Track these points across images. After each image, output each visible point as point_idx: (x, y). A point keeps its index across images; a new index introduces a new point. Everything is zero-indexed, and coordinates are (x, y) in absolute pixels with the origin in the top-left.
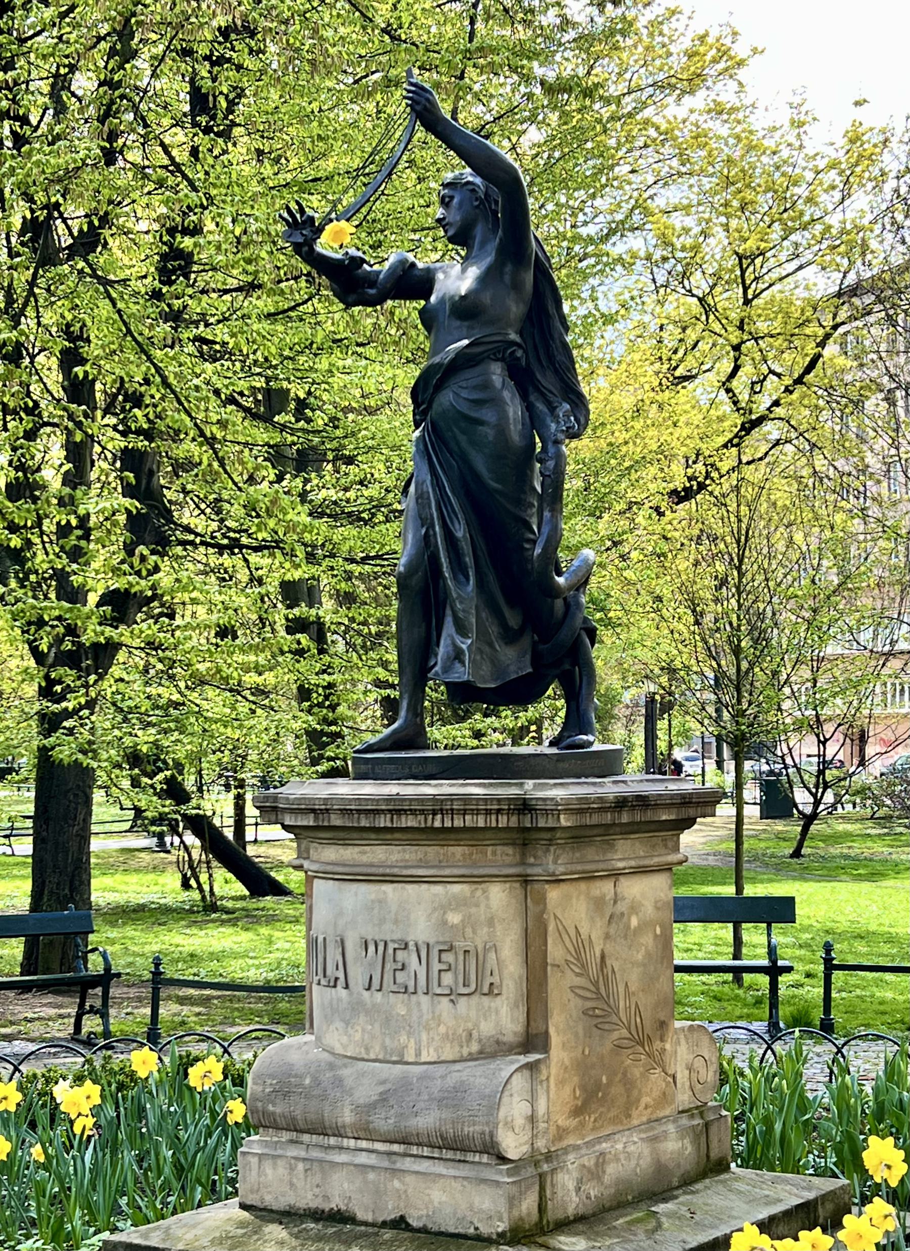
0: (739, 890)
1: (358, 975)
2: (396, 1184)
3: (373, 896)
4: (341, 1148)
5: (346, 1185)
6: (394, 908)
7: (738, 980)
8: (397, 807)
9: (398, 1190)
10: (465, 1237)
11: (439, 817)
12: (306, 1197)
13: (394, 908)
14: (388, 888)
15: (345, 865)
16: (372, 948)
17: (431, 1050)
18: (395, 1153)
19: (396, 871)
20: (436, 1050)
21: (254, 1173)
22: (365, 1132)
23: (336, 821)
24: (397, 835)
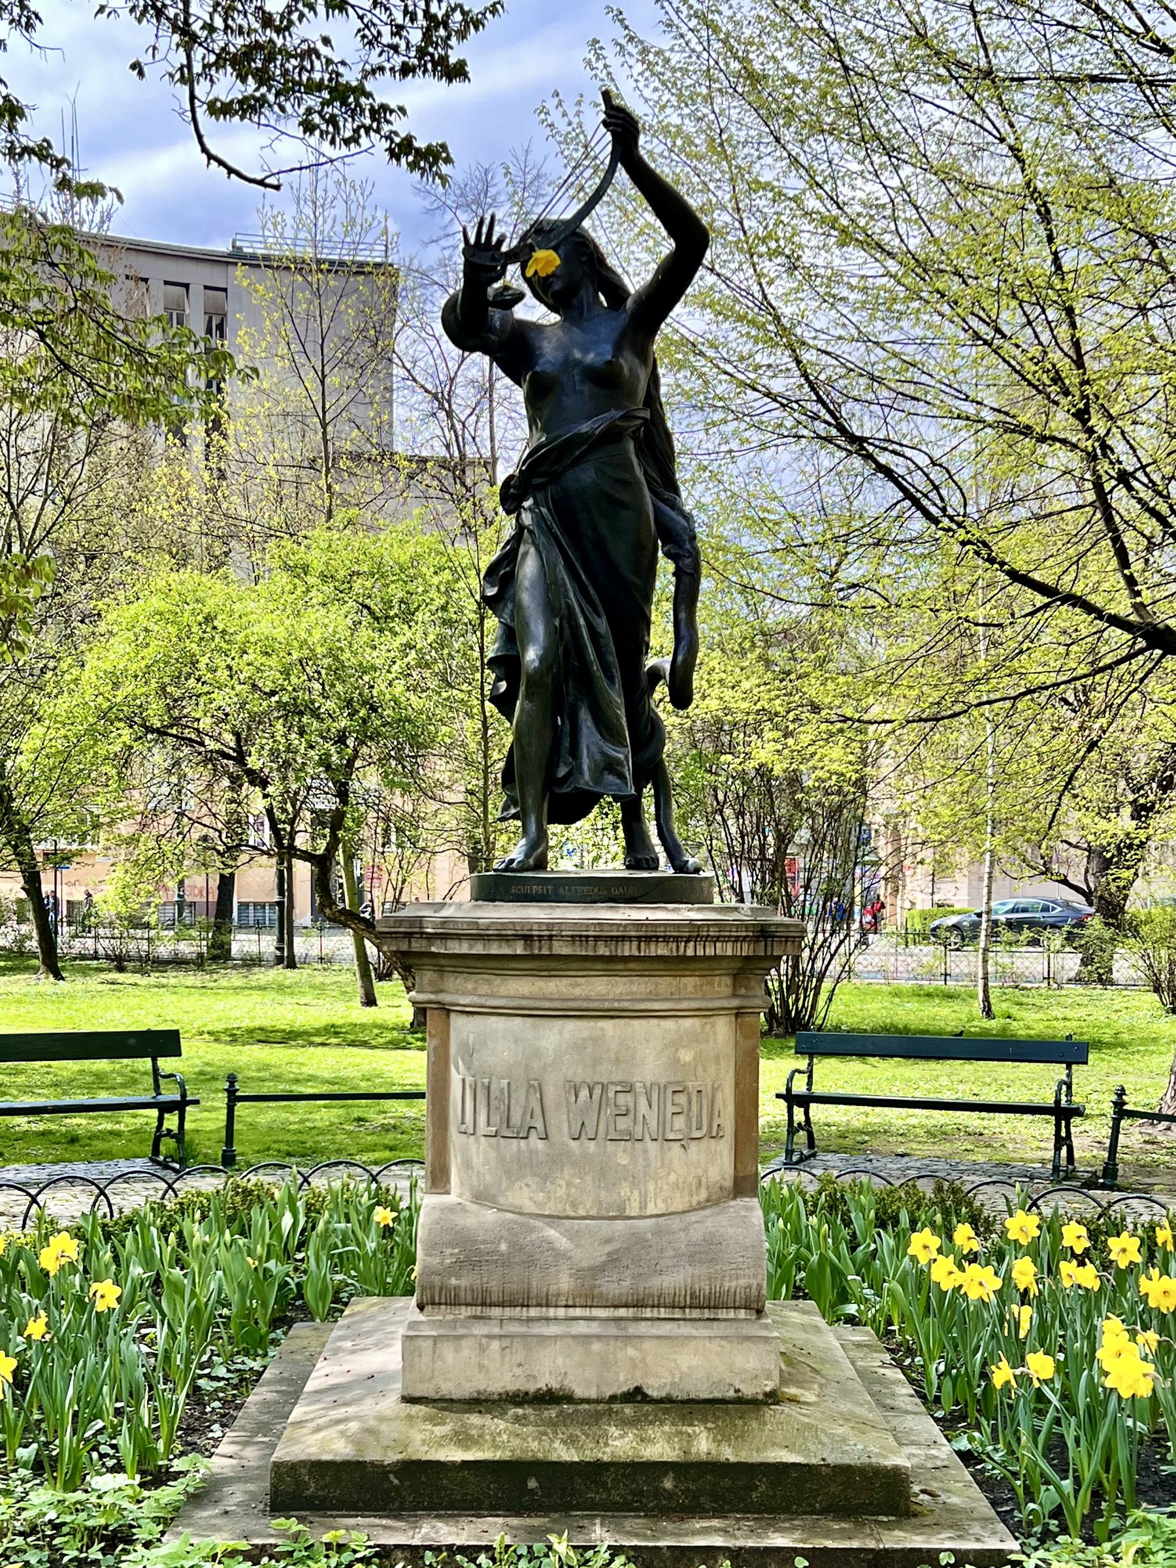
1: (561, 1126)
2: (631, 1352)
3: (585, 1034)
4: (548, 1319)
5: (560, 1361)
6: (614, 1046)
8: (648, 934)
9: (632, 1359)
10: (723, 1401)
11: (691, 944)
13: (614, 1046)
14: (607, 1025)
15: (545, 999)
16: (584, 1093)
17: (659, 1202)
18: (621, 1319)
19: (625, 1005)
20: (665, 1201)
21: (426, 1359)
22: (589, 1299)
24: (631, 965)
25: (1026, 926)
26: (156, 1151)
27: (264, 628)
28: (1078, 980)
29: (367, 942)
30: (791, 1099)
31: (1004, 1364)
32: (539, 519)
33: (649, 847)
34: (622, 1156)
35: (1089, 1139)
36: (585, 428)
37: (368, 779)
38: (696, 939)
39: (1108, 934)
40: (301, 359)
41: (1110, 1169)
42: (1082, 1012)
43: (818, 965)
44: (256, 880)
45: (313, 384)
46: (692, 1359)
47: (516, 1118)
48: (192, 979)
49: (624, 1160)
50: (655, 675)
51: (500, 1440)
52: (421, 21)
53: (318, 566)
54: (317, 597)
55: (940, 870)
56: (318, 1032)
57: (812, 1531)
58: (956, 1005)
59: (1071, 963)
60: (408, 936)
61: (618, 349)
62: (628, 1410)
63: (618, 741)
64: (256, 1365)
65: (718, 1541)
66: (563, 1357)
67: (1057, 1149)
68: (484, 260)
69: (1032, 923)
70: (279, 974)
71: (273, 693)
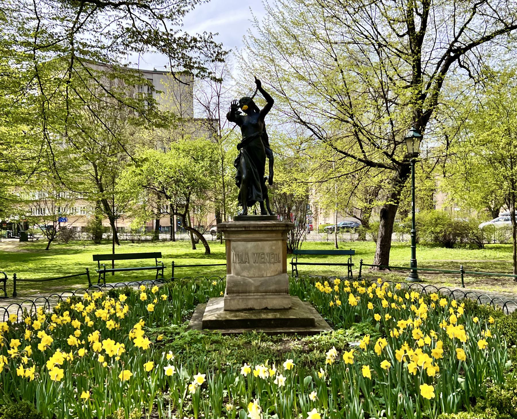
0: (113, 262)
1: (252, 261)
2: (265, 301)
7: (113, 274)
8: (267, 226)
12: (243, 306)
14: (260, 243)
16: (256, 255)
23: (251, 229)
25: (346, 228)
26: (157, 278)
27: (170, 163)
28: (358, 240)
29: (194, 234)
30: (293, 264)
31: (332, 302)
32: (244, 151)
33: (265, 210)
34: (262, 266)
35: (355, 272)
36: (252, 135)
37: (193, 197)
38: (275, 227)
39: (364, 229)
40: (176, 100)
41: (360, 276)
42: (358, 247)
43: (298, 238)
44: (165, 221)
45: (178, 106)
46: (276, 302)
47: (243, 260)
48: (151, 244)
49: (263, 267)
50: (266, 178)
51: (243, 315)
52: (217, 53)
53: (182, 148)
54: (182, 155)
55: (327, 215)
56: (183, 255)
57: (297, 330)
58: (330, 246)
59: (356, 236)
60: (223, 227)
61: (258, 121)
62: (265, 311)
63: (260, 191)
64: (192, 311)
65: (282, 331)
66: (253, 301)
67: (349, 272)
68: (234, 107)
69: (347, 227)
70: (171, 243)
71: (172, 177)
